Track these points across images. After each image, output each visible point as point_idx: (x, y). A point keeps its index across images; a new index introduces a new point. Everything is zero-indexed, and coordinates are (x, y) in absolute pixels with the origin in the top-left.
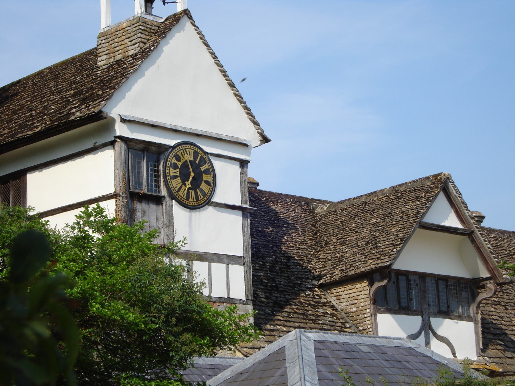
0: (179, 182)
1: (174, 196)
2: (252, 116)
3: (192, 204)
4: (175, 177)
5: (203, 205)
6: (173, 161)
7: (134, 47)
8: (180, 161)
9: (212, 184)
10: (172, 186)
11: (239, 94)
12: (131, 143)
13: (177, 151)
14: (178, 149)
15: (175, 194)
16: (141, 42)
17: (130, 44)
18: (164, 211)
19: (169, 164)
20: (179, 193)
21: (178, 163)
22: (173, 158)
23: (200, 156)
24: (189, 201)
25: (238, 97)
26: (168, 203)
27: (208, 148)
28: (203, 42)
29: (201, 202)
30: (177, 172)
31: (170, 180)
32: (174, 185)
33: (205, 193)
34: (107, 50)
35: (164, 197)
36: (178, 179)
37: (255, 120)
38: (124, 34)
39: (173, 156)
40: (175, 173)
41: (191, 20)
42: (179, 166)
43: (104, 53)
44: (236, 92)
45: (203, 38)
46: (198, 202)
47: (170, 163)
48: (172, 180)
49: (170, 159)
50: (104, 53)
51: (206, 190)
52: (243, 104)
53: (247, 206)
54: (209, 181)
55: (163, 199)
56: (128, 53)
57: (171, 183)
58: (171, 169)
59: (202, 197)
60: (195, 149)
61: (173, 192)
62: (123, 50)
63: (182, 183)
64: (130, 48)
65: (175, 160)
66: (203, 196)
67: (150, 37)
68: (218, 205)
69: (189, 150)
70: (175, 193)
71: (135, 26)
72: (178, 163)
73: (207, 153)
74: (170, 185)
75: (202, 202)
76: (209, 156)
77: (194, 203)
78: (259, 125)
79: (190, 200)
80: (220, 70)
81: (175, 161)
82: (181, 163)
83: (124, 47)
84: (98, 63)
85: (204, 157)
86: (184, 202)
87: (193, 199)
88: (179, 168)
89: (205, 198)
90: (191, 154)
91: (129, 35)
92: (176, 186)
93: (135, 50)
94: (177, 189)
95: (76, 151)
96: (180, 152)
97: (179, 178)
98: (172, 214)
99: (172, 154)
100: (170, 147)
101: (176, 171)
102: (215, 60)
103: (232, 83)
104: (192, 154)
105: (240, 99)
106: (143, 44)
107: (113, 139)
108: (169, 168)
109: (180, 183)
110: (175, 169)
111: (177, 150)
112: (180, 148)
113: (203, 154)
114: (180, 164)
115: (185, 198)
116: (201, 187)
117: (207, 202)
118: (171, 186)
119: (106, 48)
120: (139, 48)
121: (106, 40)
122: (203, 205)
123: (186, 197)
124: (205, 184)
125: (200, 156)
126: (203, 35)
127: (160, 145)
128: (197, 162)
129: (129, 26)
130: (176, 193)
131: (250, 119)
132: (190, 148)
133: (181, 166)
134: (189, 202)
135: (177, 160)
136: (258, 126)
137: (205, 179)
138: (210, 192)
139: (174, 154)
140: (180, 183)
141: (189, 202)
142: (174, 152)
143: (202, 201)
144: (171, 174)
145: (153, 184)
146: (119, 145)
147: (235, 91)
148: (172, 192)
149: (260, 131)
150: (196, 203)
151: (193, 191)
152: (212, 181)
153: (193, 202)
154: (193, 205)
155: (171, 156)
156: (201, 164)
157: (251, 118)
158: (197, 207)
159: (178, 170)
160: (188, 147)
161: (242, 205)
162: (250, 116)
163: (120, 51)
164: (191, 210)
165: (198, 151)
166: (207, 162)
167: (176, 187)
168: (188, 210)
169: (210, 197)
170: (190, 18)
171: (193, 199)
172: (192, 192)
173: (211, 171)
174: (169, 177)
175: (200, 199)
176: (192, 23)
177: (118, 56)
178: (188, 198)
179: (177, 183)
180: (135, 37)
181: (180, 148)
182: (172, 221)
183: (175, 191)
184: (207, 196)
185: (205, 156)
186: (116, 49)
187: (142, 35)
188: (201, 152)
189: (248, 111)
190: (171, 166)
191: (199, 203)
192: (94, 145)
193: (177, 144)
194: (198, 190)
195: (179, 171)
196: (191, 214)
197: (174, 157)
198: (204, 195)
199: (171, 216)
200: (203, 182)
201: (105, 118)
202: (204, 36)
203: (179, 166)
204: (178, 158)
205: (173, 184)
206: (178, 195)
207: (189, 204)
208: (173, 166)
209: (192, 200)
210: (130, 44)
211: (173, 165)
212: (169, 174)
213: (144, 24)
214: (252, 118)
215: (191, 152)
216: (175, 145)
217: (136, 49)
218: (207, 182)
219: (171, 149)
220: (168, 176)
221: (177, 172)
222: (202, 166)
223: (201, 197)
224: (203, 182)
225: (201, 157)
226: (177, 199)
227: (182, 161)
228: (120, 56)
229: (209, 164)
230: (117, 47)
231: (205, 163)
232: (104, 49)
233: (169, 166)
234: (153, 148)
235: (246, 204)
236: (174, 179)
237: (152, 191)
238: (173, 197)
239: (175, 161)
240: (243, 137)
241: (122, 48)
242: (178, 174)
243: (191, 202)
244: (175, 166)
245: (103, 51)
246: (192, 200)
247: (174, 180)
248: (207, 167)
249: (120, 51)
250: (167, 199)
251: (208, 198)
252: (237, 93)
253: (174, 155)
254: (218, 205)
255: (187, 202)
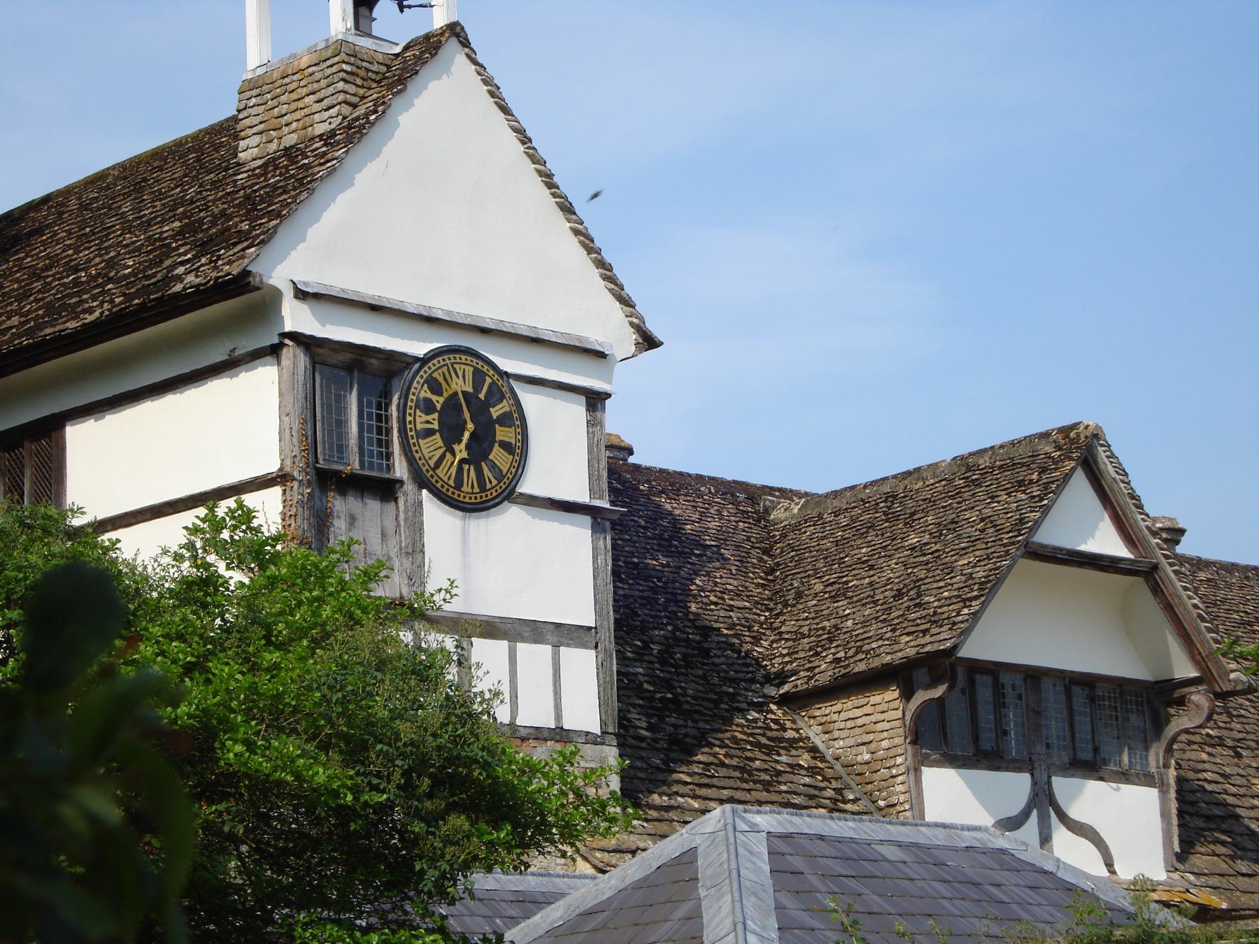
0: (438, 445)
1: (426, 480)
2: (616, 284)
3: (470, 498)
4: (429, 433)
5: (497, 501)
6: (423, 395)
7: (327, 114)
8: (440, 394)
9: (517, 451)
10: (420, 454)
11: (583, 230)
12: (321, 351)
13: (433, 368)
14: (434, 365)
15: (428, 475)
16: (346, 102)
17: (317, 107)
18: (402, 516)
19: (412, 400)
20: (438, 471)
21: (434, 398)
22: (423, 386)
23: (488, 380)
24: (463, 492)
25: (582, 238)
26: (411, 497)
27: (510, 362)
28: (496, 103)
29: (491, 494)
30: (432, 421)
31: (415, 440)
32: (425, 452)
33: (502, 472)
34: (261, 123)
35: (401, 482)
36: (435, 437)
37: (623, 293)
38: (302, 83)
39: (422, 381)
40: (428, 422)
41: (467, 50)
42: (439, 407)
43: (255, 130)
44: (577, 225)
45: (497, 93)
46: (483, 494)
47: (414, 398)
48: (420, 440)
49: (416, 388)
50: (255, 130)
51: (504, 463)
52: (595, 255)
53: (604, 504)
54: (510, 443)
55: (397, 486)
56: (313, 130)
57: (417, 448)
58: (418, 413)
59: (494, 482)
60: (477, 364)
61: (424, 469)
62: (301, 122)
63: (444, 449)
64: (317, 117)
65: (428, 391)
66: (496, 479)
67: (366, 90)
68: (532, 501)
69: (463, 366)
70: (428, 471)
71: (329, 63)
72: (434, 398)
73: (506, 375)
74: (417, 452)
75: (495, 494)
76: (511, 381)
77: (473, 496)
78: (633, 307)
79: (465, 488)
80: (538, 171)
81: (429, 395)
82: (441, 400)
83: (303, 114)
84: (240, 155)
85: (499, 384)
86: (450, 494)
87: (473, 487)
88: (437, 411)
89: (502, 484)
90: (467, 377)
91: (315, 85)
92: (431, 454)
93: (330, 123)
94: (432, 463)
95: (186, 369)
96: (440, 371)
97: (438, 436)
98: (422, 523)
99: (422, 377)
100: (417, 359)
101: (429, 418)
102: (525, 146)
103: (567, 203)
104: (469, 376)
105: (587, 242)
106: (350, 108)
107: (276, 340)
108: (412, 412)
109: (441, 447)
110: (427, 414)
111: (432, 367)
112: (439, 362)
113: (496, 376)
114: (439, 401)
115: (453, 485)
116: (491, 457)
117: (505, 494)
118: (417, 456)
119: (259, 119)
120: (340, 117)
121: (259, 98)
122: (497, 501)
123: (455, 482)
124: (502, 451)
125: (488, 380)
126: (496, 85)
127: (391, 356)
128: (482, 396)
129: (316, 65)
130: (431, 472)
131: (610, 290)
132: (464, 361)
133: (442, 405)
134: (462, 494)
135: (433, 392)
136: (631, 309)
137: (501, 438)
138: (514, 471)
139: (425, 376)
140: (441, 447)
141: (462, 494)
142: (425, 372)
143: (493, 491)
144: (419, 427)
145: (373, 450)
146: (291, 354)
147: (575, 222)
148: (421, 470)
149: (635, 321)
150: (478, 496)
151: (472, 468)
152: (518, 444)
153: (472, 493)
154: (473, 501)
155: (418, 382)
156: (491, 402)
157: (613, 289)
158: (482, 506)
159: (436, 416)
160: (460, 358)
161: (593, 501)
162: (611, 282)
163: (294, 125)
164: (468, 514)
165: (485, 370)
166: (507, 396)
167: (430, 458)
168: (460, 513)
169: (514, 483)
170: (465, 43)
171: (473, 487)
172: (469, 470)
173: (516, 417)
174: (413, 433)
175: (489, 486)
176: (468, 56)
177: (289, 136)
178: (459, 484)
179: (432, 448)
180: (331, 90)
181: (439, 362)
182: (421, 541)
183: (427, 467)
184: (505, 480)
185: (501, 382)
186: (284, 120)
187: (346, 86)
188: (491, 372)
189: (605, 272)
190: (417, 406)
191: (487, 496)
192: (229, 355)
193: (432, 353)
194: (483, 464)
195: (437, 418)
196: (467, 522)
197: (426, 385)
198: (500, 476)
199: (417, 529)
200: (496, 444)
201: (258, 289)
202: (499, 88)
203: (439, 407)
204: (435, 387)
205: (423, 449)
206: (436, 478)
207: (461, 499)
208: (422, 406)
209: (469, 490)
210: (317, 107)
211: (422, 402)
212: (412, 426)
213: (352, 59)
214: (616, 288)
215: (466, 372)
216: (429, 355)
217: (332, 120)
218: (506, 446)
219: (417, 366)
220: (411, 430)
221: (434, 419)
222: (493, 407)
223: (491, 482)
224: (496, 444)
225: (491, 385)
226: (432, 487)
227: (446, 395)
228: (294, 136)
229: (512, 402)
230: (286, 114)
231: (502, 398)
232: (255, 120)
233: (413, 405)
234: (374, 361)
235: (601, 498)
236: (424, 438)
237: (371, 467)
238: (422, 481)
239: (429, 395)
240: (594, 336)
241: (299, 117)
242: (436, 426)
243: (467, 493)
244: (428, 407)
245: (252, 125)
246: (469, 490)
247: (425, 441)
248: (507, 409)
249: (294, 125)
250: (409, 487)
251: (509, 484)
252: (580, 227)
253: (427, 378)
254: (532, 501)
255: (456, 494)
